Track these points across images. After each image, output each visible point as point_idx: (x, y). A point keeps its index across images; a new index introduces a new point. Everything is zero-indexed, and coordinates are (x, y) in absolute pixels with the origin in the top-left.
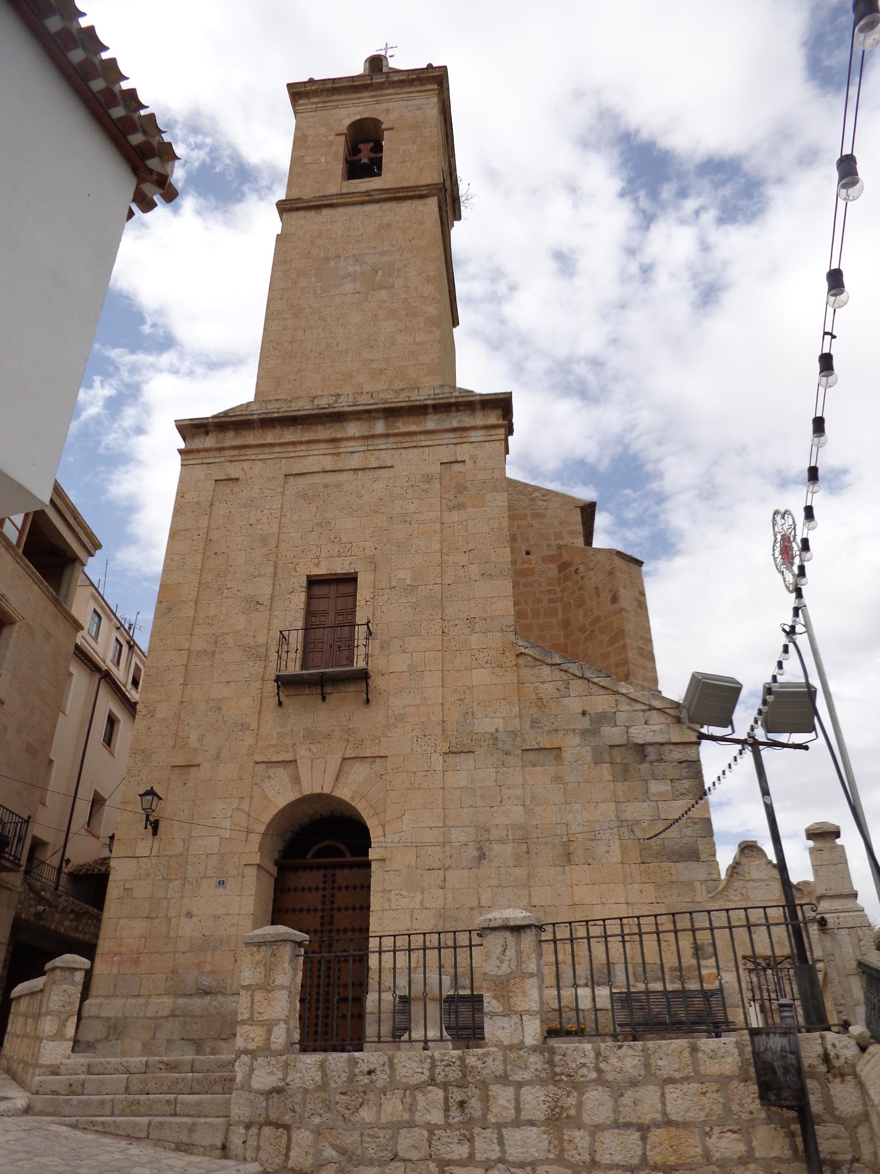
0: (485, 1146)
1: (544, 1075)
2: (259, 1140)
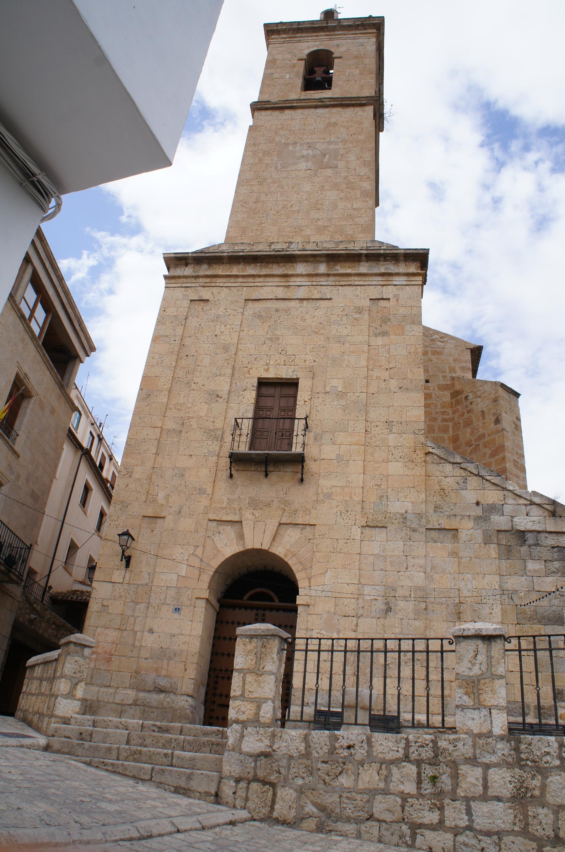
0: (454, 815)
1: (510, 759)
2: (247, 792)
